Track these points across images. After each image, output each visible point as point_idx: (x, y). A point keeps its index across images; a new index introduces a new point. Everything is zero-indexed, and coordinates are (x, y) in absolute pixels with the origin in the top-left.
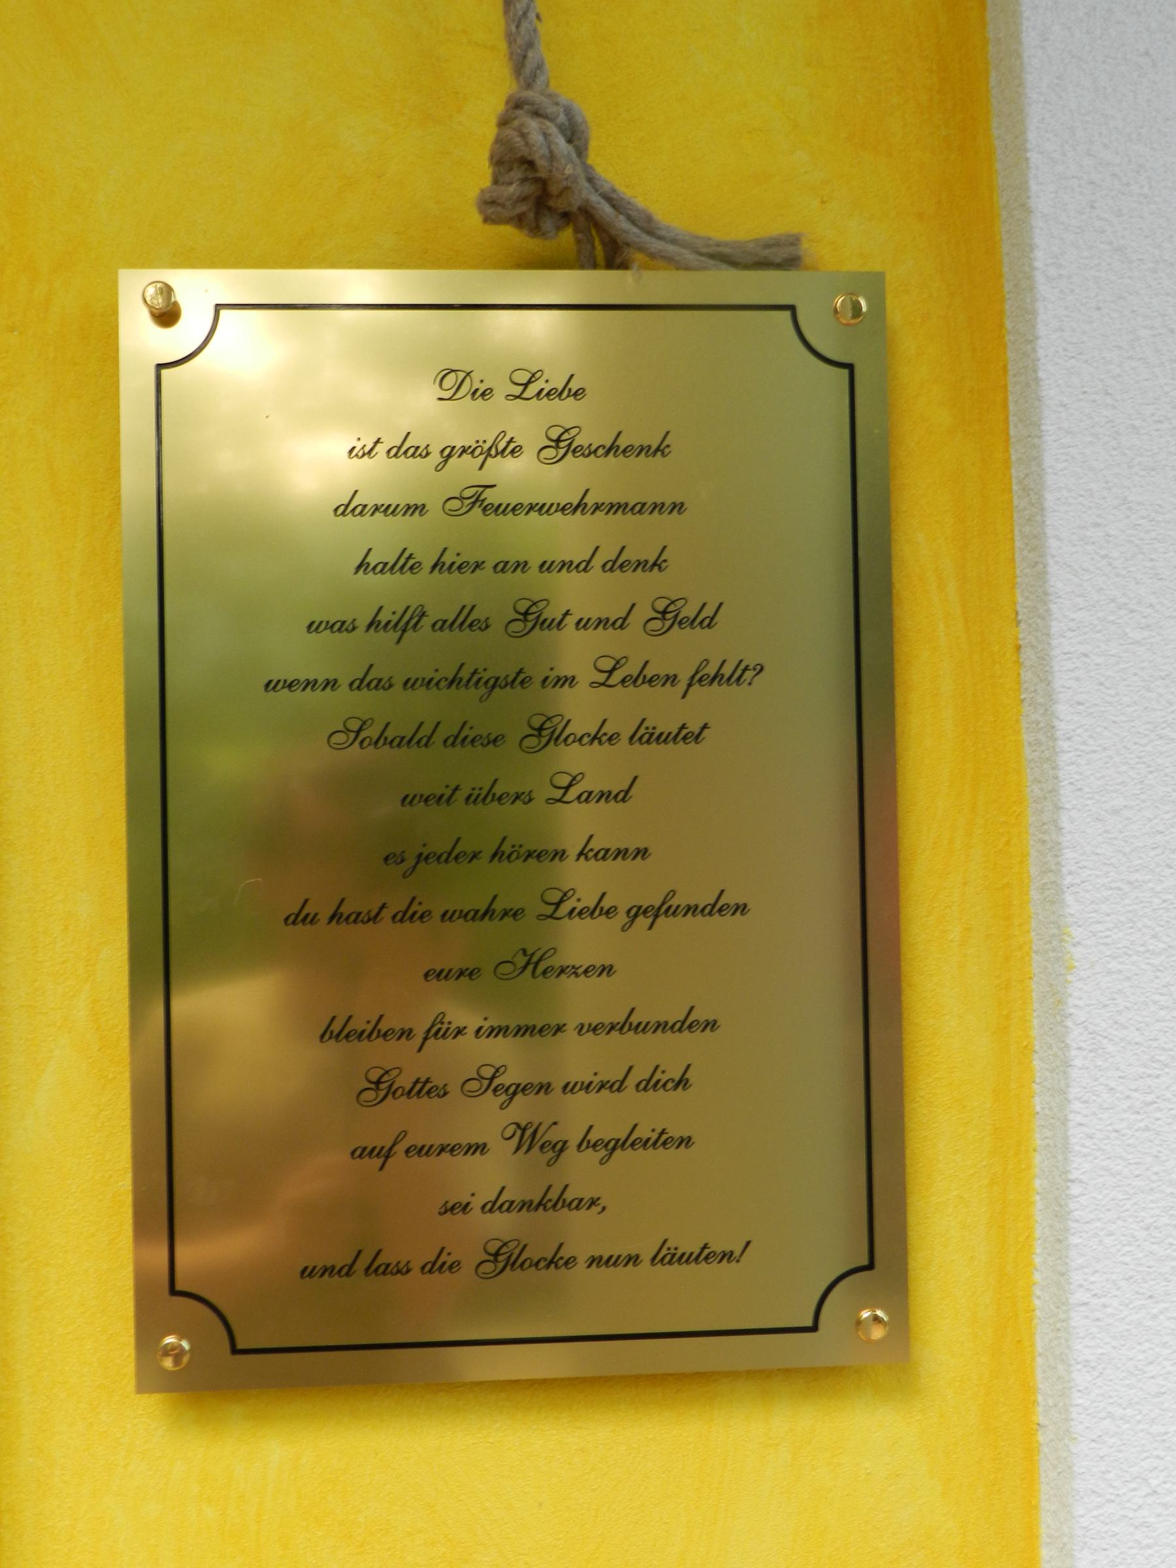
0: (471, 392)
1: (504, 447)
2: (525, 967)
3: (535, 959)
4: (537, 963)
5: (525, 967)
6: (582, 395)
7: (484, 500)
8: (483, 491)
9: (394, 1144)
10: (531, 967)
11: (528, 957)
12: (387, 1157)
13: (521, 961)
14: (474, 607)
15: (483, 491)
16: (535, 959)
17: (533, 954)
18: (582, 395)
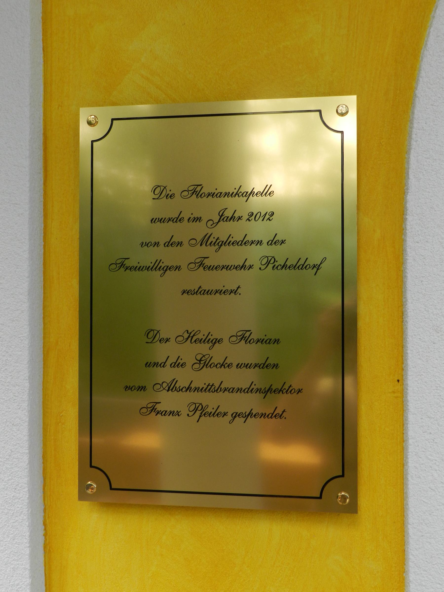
0: (159, 340)
1: (241, 332)
2: (187, 339)
3: (192, 335)
4: (192, 337)
5: (187, 339)
6: (174, 197)
7: (204, 264)
8: (204, 260)
9: (321, 263)
10: (190, 338)
11: (189, 334)
12: (318, 269)
13: (186, 335)
14: (271, 185)
15: (204, 260)
16: (192, 335)
17: (191, 333)
18: (174, 197)
